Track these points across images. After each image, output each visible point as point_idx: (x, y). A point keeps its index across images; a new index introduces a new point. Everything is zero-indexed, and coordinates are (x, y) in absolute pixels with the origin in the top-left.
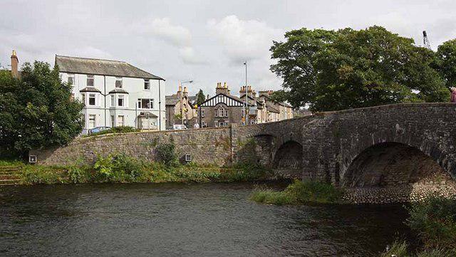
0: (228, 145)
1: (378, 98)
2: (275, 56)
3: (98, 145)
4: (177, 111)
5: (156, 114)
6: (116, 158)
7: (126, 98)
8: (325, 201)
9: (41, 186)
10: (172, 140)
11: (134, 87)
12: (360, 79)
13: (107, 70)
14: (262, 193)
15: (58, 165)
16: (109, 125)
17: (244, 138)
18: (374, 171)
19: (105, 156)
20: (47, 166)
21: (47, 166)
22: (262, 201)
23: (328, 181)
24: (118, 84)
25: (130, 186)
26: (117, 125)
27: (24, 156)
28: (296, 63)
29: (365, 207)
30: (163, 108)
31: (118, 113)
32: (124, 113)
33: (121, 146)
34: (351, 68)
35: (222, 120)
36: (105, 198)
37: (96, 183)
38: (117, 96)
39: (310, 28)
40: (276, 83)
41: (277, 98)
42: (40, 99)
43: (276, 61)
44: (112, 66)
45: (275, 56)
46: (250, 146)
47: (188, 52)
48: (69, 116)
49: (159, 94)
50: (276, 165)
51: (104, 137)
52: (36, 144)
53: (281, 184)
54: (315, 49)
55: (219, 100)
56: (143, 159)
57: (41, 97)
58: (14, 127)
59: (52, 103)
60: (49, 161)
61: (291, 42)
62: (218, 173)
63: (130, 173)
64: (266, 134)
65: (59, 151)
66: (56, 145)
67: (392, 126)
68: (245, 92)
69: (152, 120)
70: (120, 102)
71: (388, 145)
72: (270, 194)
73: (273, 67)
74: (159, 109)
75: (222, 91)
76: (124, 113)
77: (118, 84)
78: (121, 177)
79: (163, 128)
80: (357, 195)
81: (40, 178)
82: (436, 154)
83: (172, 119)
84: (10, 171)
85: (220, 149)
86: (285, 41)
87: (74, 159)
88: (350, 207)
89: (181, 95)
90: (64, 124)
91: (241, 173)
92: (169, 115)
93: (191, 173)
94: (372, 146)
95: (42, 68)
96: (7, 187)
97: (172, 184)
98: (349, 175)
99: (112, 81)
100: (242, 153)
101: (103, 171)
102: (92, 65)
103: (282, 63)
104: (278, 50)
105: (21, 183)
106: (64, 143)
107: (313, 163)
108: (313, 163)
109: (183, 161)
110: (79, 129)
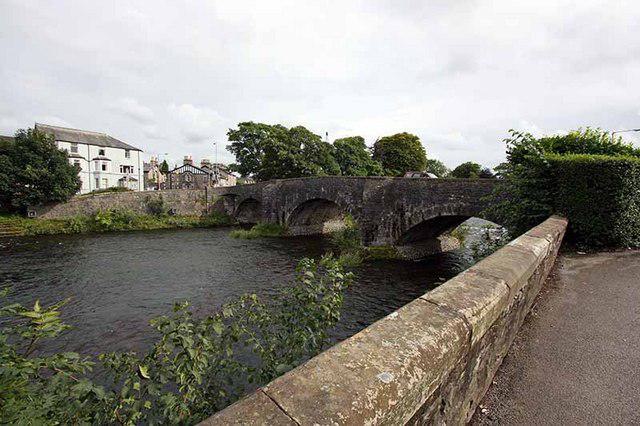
0: (204, 199)
1: (297, 172)
2: (230, 139)
3: (96, 202)
4: (150, 176)
5: (137, 178)
6: (114, 211)
7: (108, 164)
8: (277, 234)
9: (44, 236)
10: (161, 198)
11: (115, 156)
12: (291, 160)
13: (90, 140)
14: (236, 232)
15: (58, 218)
16: (93, 187)
17: (216, 197)
18: (305, 216)
19: (104, 209)
20: (46, 219)
21: (46, 219)
22: (238, 237)
23: (278, 223)
24: (102, 153)
25: (127, 233)
26: (103, 186)
27: (23, 212)
28: (245, 145)
29: (300, 238)
30: (142, 173)
31: (102, 176)
32: (108, 176)
33: (118, 203)
34: (286, 153)
35: (188, 184)
36: (106, 241)
37: (97, 230)
38: (101, 163)
39: (256, 122)
40: (230, 159)
41: (233, 167)
42: (39, 163)
43: (230, 143)
44: (94, 137)
45: (230, 139)
46: (220, 202)
47: (152, 129)
48: (70, 178)
49: (136, 161)
50: (238, 215)
51: (102, 195)
52: (35, 202)
53: (247, 226)
54: (258, 137)
55: (187, 168)
56: (140, 213)
57: (39, 161)
58: (10, 186)
59: (52, 166)
60: (47, 216)
61: (242, 130)
62: (198, 221)
63: (127, 223)
64: (230, 194)
65: (59, 206)
66: (58, 201)
67: (318, 189)
68: (205, 164)
69: (133, 183)
70: (104, 168)
71: (317, 200)
72: (242, 232)
73: (228, 147)
74: (138, 174)
75: (188, 163)
76: (108, 176)
77: (102, 153)
78: (121, 226)
79: (142, 190)
80: (295, 231)
81: (43, 229)
82: (344, 204)
83: (149, 183)
84: (8, 225)
85: (198, 204)
86: (238, 129)
87: (74, 213)
88: (293, 238)
89: (154, 163)
90: (60, 179)
91: (214, 220)
92: (145, 178)
93: (177, 221)
94: (307, 202)
95: (57, 134)
96: (5, 239)
97: (164, 230)
98: (291, 219)
99: (95, 151)
100: (214, 207)
101: (104, 222)
102: (75, 135)
103: (234, 145)
104: (233, 135)
105: (23, 234)
106: (64, 199)
107: (269, 212)
108: (269, 212)
109: (170, 213)
110: (78, 188)
